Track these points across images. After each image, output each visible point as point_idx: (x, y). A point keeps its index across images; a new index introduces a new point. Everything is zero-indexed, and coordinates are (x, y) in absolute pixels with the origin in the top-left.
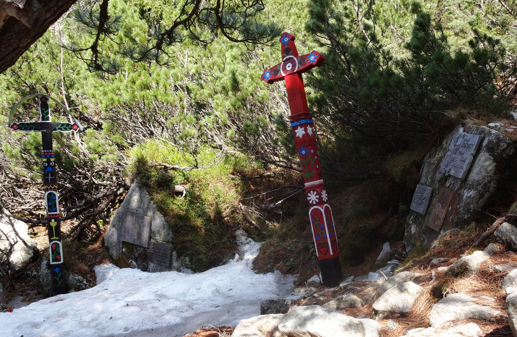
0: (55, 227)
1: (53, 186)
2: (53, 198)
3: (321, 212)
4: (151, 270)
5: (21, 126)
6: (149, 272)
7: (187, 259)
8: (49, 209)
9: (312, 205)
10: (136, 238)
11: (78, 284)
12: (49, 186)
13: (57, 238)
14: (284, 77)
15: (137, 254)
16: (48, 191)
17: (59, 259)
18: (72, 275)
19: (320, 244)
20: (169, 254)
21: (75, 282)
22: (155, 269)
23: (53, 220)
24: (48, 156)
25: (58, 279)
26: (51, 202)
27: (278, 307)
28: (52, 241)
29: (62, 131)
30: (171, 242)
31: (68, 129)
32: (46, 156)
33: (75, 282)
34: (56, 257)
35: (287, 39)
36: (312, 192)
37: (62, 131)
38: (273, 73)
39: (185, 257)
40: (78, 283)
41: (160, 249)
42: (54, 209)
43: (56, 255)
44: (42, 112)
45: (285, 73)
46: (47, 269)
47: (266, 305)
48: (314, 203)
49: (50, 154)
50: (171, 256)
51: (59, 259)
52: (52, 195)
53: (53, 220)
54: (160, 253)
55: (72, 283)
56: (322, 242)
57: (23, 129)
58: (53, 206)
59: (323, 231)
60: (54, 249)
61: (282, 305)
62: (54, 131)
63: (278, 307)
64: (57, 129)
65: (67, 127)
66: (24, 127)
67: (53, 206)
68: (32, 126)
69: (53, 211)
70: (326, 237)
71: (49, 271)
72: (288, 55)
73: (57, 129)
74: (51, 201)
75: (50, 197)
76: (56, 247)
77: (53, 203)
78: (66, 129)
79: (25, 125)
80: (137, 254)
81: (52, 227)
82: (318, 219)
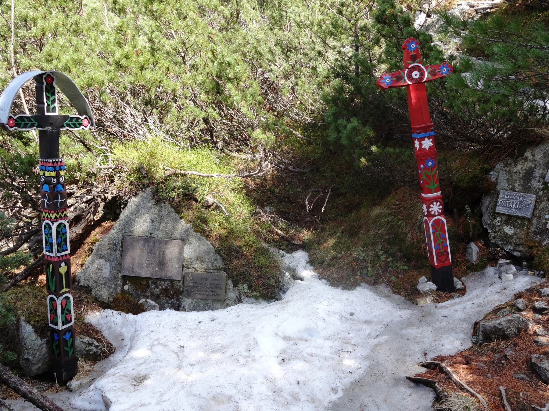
0: (65, 273)
1: (62, 213)
2: (63, 231)
3: (443, 222)
4: (186, 308)
5: (20, 122)
6: (184, 310)
7: (246, 286)
8: (59, 248)
9: (434, 216)
10: (157, 269)
11: (87, 349)
12: (58, 214)
13: (68, 289)
14: (409, 85)
15: (158, 290)
16: (56, 221)
17: (69, 319)
18: (78, 339)
19: (440, 253)
20: (224, 284)
21: (84, 346)
22: (194, 306)
23: (63, 264)
24: (58, 168)
25: (68, 350)
26: (61, 237)
27: (516, 325)
28: (62, 296)
29: (71, 129)
30: (222, 268)
31: (77, 125)
32: (55, 167)
33: (84, 346)
34: (66, 318)
35: (414, 46)
36: (435, 203)
37: (71, 129)
38: (395, 79)
39: (243, 284)
40: (87, 347)
41: (207, 280)
42: (64, 248)
43: (67, 314)
44: (47, 99)
45: (410, 81)
46: (39, 338)
47: (505, 325)
48: (437, 213)
49: (59, 164)
50: (227, 285)
51: (69, 319)
52: (62, 225)
53: (63, 264)
54: (206, 284)
55: (79, 349)
56: (442, 251)
57: (22, 125)
58: (63, 243)
59: (443, 240)
60: (64, 305)
61: (518, 322)
62: (61, 129)
63: (516, 325)
64: (65, 125)
65: (70, 123)
66: (23, 123)
67: (63, 243)
68: (34, 122)
69: (63, 251)
70: (447, 246)
71: (44, 340)
72: (414, 62)
73: (65, 125)
74: (61, 235)
75: (60, 230)
76: (66, 303)
77: (63, 238)
78: (76, 127)
79: (25, 119)
80: (158, 290)
81: (61, 275)
82: (439, 229)
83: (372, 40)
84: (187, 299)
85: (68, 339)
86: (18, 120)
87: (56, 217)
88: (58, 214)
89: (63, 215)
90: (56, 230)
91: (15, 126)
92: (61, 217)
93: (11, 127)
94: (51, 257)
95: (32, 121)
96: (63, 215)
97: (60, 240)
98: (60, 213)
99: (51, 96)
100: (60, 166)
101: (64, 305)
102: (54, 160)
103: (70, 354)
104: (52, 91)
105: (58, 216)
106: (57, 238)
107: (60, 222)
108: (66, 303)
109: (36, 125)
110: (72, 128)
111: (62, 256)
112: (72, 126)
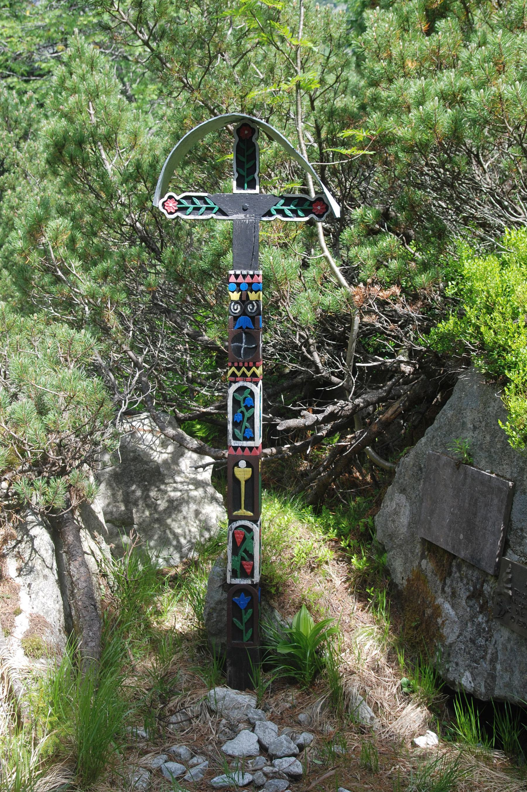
2: (249, 403)
16: (235, 382)
23: (242, 463)
25: (242, 627)
26: (242, 412)
34: (242, 566)
51: (249, 571)
60: (239, 541)
64: (274, 212)
68: (212, 205)
69: (245, 439)
73: (274, 212)
74: (243, 409)
75: (240, 398)
77: (247, 415)
81: (237, 482)
83: (82, 47)
84: (502, 629)
85: (242, 607)
86: (183, 201)
87: (234, 374)
88: (238, 369)
89: (249, 374)
90: (233, 396)
91: (176, 211)
92: (244, 375)
93: (171, 213)
94: (251, 448)
95: (195, 204)
96: (249, 374)
97: (239, 418)
98: (244, 369)
99: (248, 162)
100: (250, 284)
101: (239, 541)
102: (238, 272)
103: (246, 639)
104: (250, 151)
105: (239, 374)
106: (234, 412)
107: (241, 384)
108: (244, 539)
109: (214, 211)
110: (287, 216)
111: (243, 448)
112: (288, 213)
